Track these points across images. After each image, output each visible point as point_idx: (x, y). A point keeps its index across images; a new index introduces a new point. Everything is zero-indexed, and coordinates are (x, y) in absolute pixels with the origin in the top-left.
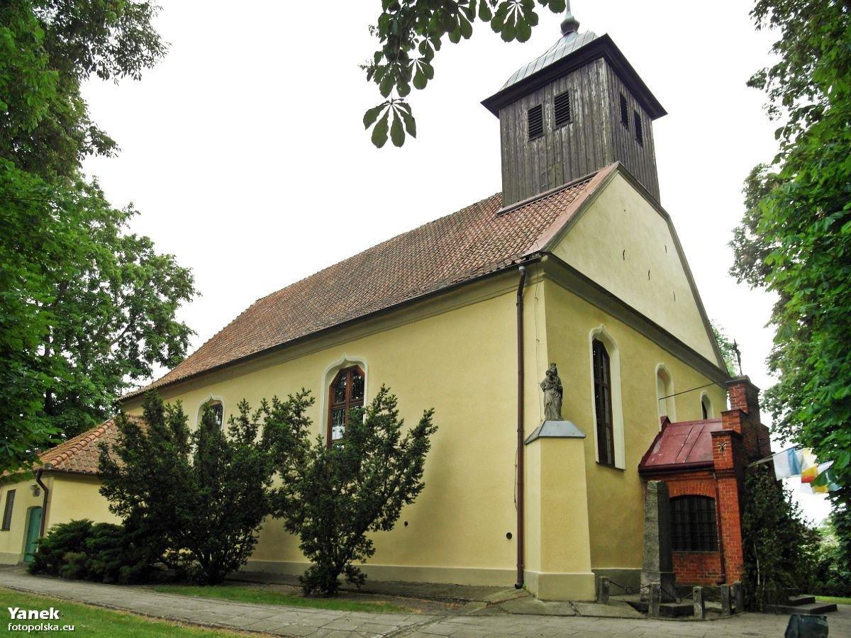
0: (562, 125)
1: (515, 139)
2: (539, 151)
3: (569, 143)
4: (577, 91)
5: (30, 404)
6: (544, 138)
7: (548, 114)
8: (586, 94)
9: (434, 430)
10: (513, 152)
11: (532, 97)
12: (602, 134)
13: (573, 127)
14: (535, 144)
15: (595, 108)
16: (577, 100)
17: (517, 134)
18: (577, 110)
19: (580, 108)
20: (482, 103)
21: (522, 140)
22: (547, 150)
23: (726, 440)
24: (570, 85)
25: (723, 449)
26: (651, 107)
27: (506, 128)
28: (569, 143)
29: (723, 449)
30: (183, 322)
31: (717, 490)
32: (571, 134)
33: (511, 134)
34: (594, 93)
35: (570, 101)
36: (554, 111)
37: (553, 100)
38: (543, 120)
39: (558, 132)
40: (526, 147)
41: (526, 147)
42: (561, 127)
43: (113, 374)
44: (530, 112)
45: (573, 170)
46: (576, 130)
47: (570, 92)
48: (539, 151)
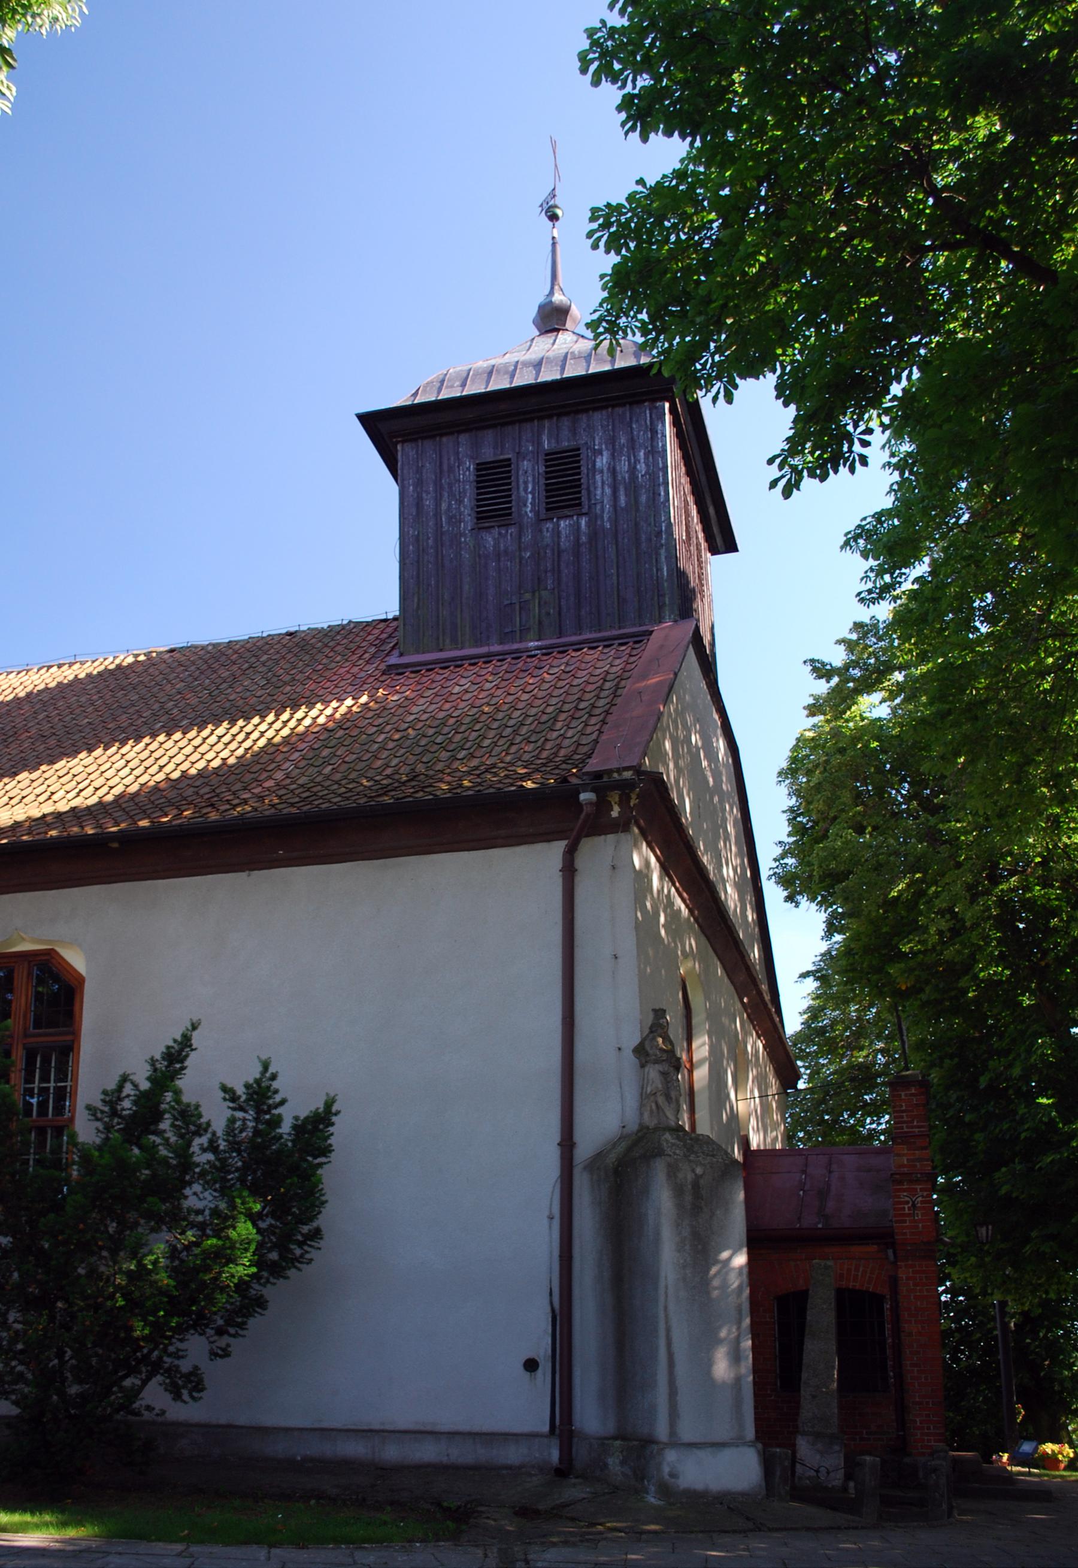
0: (560, 512)
1: (437, 515)
2: (499, 555)
3: (577, 554)
4: (600, 452)
5: (818, 1457)
6: (512, 530)
7: (526, 483)
8: (623, 466)
9: (337, 1113)
10: (430, 542)
11: (489, 436)
12: (658, 554)
13: (588, 525)
14: (489, 540)
15: (643, 498)
16: (602, 472)
17: (444, 506)
18: (599, 492)
19: (608, 491)
20: (369, 421)
21: (455, 520)
22: (521, 558)
23: (921, 1190)
24: (583, 439)
25: (914, 1205)
26: (716, 529)
27: (416, 486)
28: (577, 554)
29: (914, 1205)
30: (784, 812)
31: (894, 1281)
32: (584, 539)
33: (428, 502)
34: (642, 467)
35: (584, 469)
36: (542, 481)
37: (542, 457)
38: (514, 493)
39: (549, 525)
40: (467, 540)
41: (467, 540)
42: (559, 518)
43: (824, 1097)
44: (480, 467)
45: (583, 613)
46: (595, 534)
47: (583, 451)
48: (499, 555)
